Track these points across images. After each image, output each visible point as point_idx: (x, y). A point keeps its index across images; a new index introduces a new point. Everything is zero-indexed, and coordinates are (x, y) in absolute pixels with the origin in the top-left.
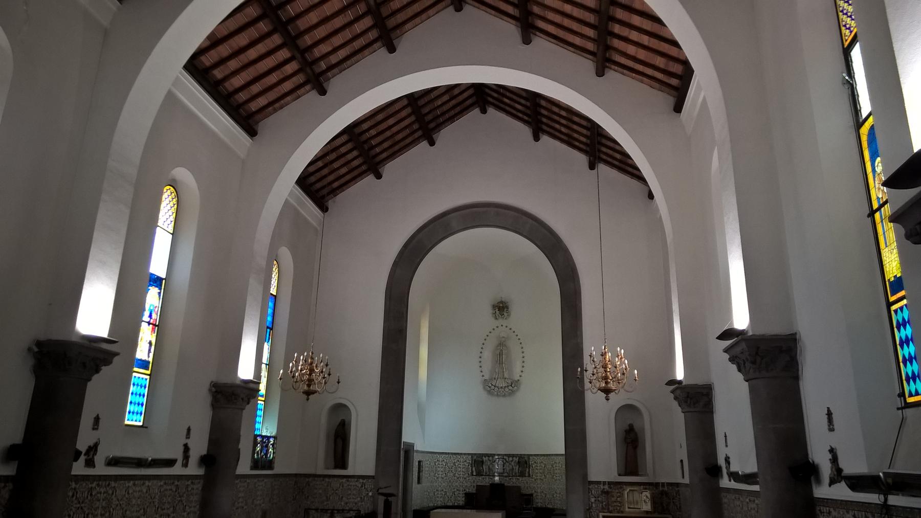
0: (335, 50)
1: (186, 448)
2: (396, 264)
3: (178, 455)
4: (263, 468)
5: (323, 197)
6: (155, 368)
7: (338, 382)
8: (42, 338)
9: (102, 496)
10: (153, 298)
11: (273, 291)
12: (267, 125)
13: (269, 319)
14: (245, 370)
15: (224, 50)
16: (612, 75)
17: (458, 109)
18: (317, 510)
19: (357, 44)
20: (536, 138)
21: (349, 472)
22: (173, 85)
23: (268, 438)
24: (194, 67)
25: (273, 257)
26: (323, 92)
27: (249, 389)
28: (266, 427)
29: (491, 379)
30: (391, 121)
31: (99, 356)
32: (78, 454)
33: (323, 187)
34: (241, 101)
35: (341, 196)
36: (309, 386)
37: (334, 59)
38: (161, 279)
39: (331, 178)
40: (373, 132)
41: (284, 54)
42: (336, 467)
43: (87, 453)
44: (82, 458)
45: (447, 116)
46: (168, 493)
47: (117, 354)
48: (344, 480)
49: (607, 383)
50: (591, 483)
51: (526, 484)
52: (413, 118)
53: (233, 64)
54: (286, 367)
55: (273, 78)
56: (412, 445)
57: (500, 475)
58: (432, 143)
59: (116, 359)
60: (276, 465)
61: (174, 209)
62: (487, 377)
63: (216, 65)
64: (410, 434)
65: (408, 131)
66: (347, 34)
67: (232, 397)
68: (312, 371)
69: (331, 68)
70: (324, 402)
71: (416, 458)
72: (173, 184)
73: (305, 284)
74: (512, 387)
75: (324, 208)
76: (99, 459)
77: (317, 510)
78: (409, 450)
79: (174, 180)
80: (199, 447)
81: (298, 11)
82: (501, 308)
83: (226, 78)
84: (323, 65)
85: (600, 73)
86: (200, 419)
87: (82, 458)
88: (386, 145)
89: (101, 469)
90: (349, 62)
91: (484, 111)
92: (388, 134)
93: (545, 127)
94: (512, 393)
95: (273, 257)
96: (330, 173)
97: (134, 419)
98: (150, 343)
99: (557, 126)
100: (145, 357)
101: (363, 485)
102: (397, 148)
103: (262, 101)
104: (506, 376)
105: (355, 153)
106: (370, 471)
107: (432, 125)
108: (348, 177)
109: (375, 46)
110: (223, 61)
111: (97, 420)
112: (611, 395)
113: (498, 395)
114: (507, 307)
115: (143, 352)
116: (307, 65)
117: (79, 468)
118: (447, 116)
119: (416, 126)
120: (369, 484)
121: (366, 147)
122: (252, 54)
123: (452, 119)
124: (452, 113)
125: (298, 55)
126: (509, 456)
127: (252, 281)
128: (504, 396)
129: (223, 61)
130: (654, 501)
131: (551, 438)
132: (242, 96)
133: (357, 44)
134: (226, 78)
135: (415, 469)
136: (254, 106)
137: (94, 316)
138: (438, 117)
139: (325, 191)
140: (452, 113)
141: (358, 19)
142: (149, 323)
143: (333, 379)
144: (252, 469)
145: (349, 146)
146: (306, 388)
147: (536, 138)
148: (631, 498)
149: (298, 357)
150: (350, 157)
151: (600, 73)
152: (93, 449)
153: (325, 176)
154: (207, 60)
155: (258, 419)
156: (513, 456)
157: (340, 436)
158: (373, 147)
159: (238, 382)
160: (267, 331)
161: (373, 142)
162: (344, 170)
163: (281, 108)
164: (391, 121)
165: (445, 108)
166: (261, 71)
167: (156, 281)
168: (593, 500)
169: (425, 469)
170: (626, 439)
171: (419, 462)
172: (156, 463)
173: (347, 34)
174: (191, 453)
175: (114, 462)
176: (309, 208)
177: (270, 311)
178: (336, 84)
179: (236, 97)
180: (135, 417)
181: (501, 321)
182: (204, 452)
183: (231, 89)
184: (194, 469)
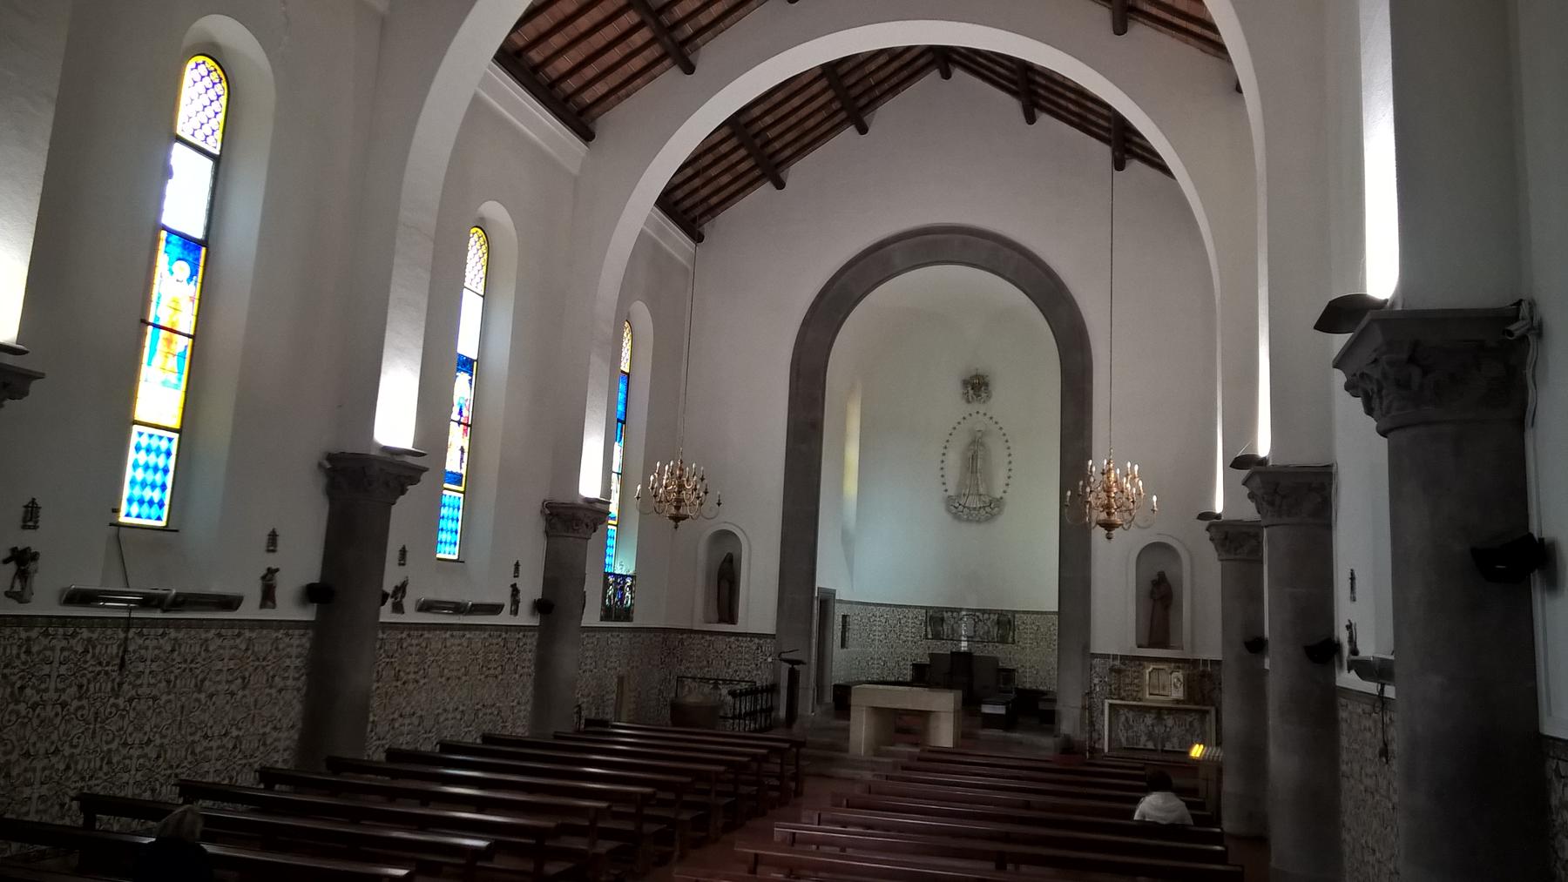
1: (515, 591)
2: (806, 323)
3: (505, 598)
4: (618, 619)
5: (694, 220)
6: (470, 482)
8: (334, 451)
9: (414, 650)
10: (463, 388)
11: (625, 367)
12: (610, 123)
13: (621, 408)
14: (589, 485)
16: (1140, 31)
17: (905, 73)
18: (694, 678)
20: (1031, 119)
21: (739, 628)
23: (624, 577)
24: (510, 58)
25: (623, 316)
26: (689, 69)
27: (595, 513)
28: (622, 563)
29: (958, 496)
30: (796, 102)
31: (403, 473)
32: (385, 596)
33: (695, 206)
34: (569, 91)
35: (724, 217)
36: (678, 508)
38: (472, 361)
39: (704, 192)
40: (768, 120)
42: (721, 621)
43: (394, 595)
45: (886, 86)
46: (494, 648)
47: (425, 470)
49: (1109, 514)
50: (1095, 656)
51: (1005, 655)
52: (830, 94)
53: (557, 41)
54: (645, 482)
55: (615, 54)
56: (833, 593)
57: (970, 639)
58: (863, 130)
60: (635, 615)
61: (483, 261)
62: (952, 492)
64: (828, 575)
65: (824, 114)
67: (572, 522)
68: (681, 487)
69: (700, 32)
70: (699, 532)
71: (839, 611)
73: (672, 353)
74: (990, 509)
75: (697, 237)
77: (694, 678)
78: (827, 599)
79: (482, 219)
80: (532, 589)
82: (977, 386)
84: (688, 29)
85: (1120, 28)
86: (531, 549)
87: (390, 601)
88: (789, 137)
89: (411, 616)
90: (727, 21)
91: (946, 75)
92: (793, 120)
93: (1043, 103)
94: (991, 517)
95: (623, 316)
96: (704, 185)
97: (448, 551)
98: (462, 450)
99: (1063, 102)
101: (759, 646)
102: (807, 140)
103: (601, 88)
104: (982, 490)
105: (742, 152)
106: (770, 628)
107: (863, 102)
108: (733, 188)
111: (403, 552)
112: (1114, 532)
113: (968, 520)
114: (987, 385)
115: (454, 463)
116: (664, 32)
117: (386, 614)
118: (886, 86)
119: (836, 105)
120: (769, 646)
121: (758, 142)
123: (894, 90)
124: (895, 80)
125: (650, 20)
126: (984, 611)
127: (594, 359)
128: (978, 521)
130: (1189, 685)
131: (1038, 589)
132: (571, 85)
135: (838, 627)
136: (588, 97)
138: (872, 88)
139: (698, 212)
140: (895, 80)
142: (459, 423)
143: (710, 501)
145: (734, 142)
146: (673, 511)
147: (1031, 119)
148: (1155, 681)
149: (662, 467)
150: (734, 158)
151: (1120, 28)
152: (401, 589)
153: (696, 190)
155: (609, 551)
156: (990, 612)
157: (725, 580)
158: (769, 142)
159: (580, 502)
160: (618, 426)
161: (770, 134)
162: (725, 179)
163: (628, 95)
164: (796, 102)
165: (882, 74)
166: (598, 46)
167: (466, 364)
168: (1096, 681)
169: (853, 626)
170: (1152, 593)
171: (844, 617)
172: (478, 609)
174: (521, 596)
175: (426, 607)
176: (676, 240)
177: (621, 397)
178: (709, 55)
180: (448, 548)
181: (975, 407)
182: (539, 596)
183: (554, 75)
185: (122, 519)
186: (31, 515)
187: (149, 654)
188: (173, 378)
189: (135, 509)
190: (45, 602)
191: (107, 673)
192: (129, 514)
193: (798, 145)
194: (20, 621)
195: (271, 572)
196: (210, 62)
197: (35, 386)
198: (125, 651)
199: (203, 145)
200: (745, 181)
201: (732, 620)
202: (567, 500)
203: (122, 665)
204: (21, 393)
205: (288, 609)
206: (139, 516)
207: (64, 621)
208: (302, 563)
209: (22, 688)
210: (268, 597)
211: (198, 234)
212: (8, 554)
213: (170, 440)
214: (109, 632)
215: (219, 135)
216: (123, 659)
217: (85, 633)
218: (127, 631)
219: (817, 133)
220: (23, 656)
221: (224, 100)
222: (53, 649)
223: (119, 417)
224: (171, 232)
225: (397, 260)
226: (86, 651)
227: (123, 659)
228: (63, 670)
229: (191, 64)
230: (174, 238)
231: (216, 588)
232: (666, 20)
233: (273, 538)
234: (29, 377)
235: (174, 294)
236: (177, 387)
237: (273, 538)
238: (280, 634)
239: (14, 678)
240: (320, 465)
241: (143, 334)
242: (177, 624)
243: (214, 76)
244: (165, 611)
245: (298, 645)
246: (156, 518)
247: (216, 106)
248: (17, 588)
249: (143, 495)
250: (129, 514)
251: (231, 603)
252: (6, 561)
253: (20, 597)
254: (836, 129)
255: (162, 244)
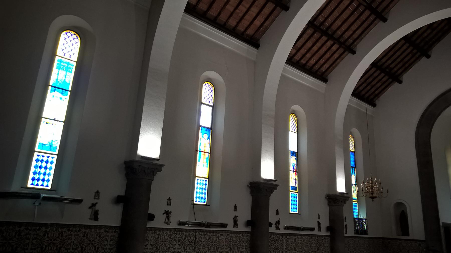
0: (354, 32)
1: (319, 224)
3: (315, 226)
6: (299, 189)
7: (388, 192)
8: (251, 181)
10: (293, 161)
12: (332, 76)
15: (303, 51)
19: (365, 25)
22: (283, 71)
23: (362, 219)
24: (290, 61)
28: (359, 213)
30: (398, 53)
32: (271, 225)
34: (317, 69)
35: (382, 97)
36: (372, 194)
37: (355, 36)
38: (296, 153)
41: (330, 43)
42: (403, 235)
44: (274, 226)
47: (278, 185)
48: (408, 242)
53: (308, 55)
55: (328, 55)
59: (278, 187)
60: (369, 232)
63: (332, 46)
65: (410, 55)
66: (359, 23)
67: (338, 202)
68: (372, 187)
69: (355, 40)
72: (294, 112)
73: (369, 144)
75: (374, 105)
76: (281, 226)
80: (325, 223)
81: (330, 23)
83: (307, 62)
86: (324, 210)
88: (399, 66)
89: (282, 231)
90: (364, 35)
92: (399, 60)
95: (347, 133)
98: (295, 179)
100: (294, 185)
102: (407, 65)
103: (326, 66)
106: (423, 238)
108: (383, 87)
109: (376, 22)
110: (304, 56)
111: (277, 211)
117: (272, 230)
122: (315, 48)
123: (438, 40)
129: (304, 56)
132: (317, 67)
133: (365, 25)
134: (307, 62)
136: (323, 69)
137: (267, 171)
141: (361, 14)
142: (293, 171)
144: (355, 234)
146: (371, 195)
150: (380, 77)
152: (278, 223)
154: (297, 58)
159: (338, 194)
162: (379, 85)
164: (398, 53)
166: (322, 54)
173: (359, 23)
174: (321, 225)
175: (287, 228)
176: (364, 106)
178: (359, 48)
179: (314, 68)
180: (294, 210)
183: (311, 66)
184: (324, 232)
185: (195, 203)
186: (169, 202)
187: (202, 240)
188: (206, 164)
189: (198, 200)
190: (174, 225)
191: (191, 245)
192: (197, 201)
193: (404, 68)
194: (168, 229)
195: (236, 217)
196: (209, 83)
197: (163, 168)
198: (196, 238)
199: (209, 104)
200: (386, 84)
201: (408, 235)
202: (333, 193)
203: (195, 243)
204: (160, 170)
205: (242, 228)
206: (199, 202)
207: (179, 230)
208: (245, 214)
209: (169, 248)
210: (235, 224)
211: (210, 126)
212: (164, 212)
213: (206, 181)
214: (191, 233)
215: (213, 101)
216: (195, 241)
217: (185, 233)
218: (196, 233)
219: (409, 63)
220: (169, 239)
221: (213, 92)
222: (177, 237)
223: (192, 176)
224: (202, 127)
225: (263, 125)
226: (185, 238)
227: (195, 241)
228: (179, 243)
229: (204, 84)
230: (203, 128)
231: (220, 221)
232: (342, 40)
233: (235, 207)
234: (162, 166)
235: (204, 143)
236: (207, 167)
237: (235, 207)
238: (296, 237)
239: (95, 245)
240: (248, 186)
241: (197, 153)
242: (210, 231)
243: (210, 86)
244: (206, 228)
245: (246, 239)
246: (203, 202)
247: (211, 94)
248: (167, 221)
249: (200, 195)
250: (197, 201)
251: (224, 226)
252: (164, 214)
253: (167, 223)
254: (418, 59)
255: (200, 130)
